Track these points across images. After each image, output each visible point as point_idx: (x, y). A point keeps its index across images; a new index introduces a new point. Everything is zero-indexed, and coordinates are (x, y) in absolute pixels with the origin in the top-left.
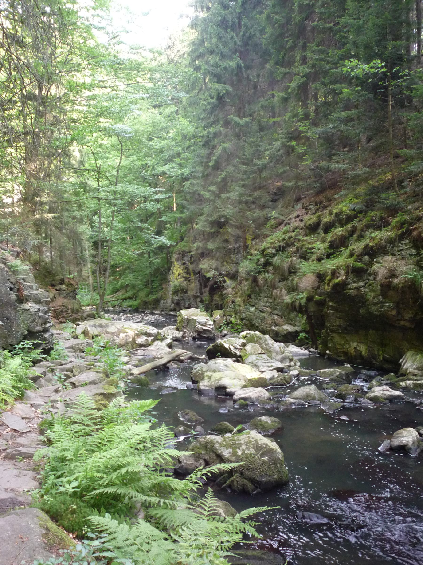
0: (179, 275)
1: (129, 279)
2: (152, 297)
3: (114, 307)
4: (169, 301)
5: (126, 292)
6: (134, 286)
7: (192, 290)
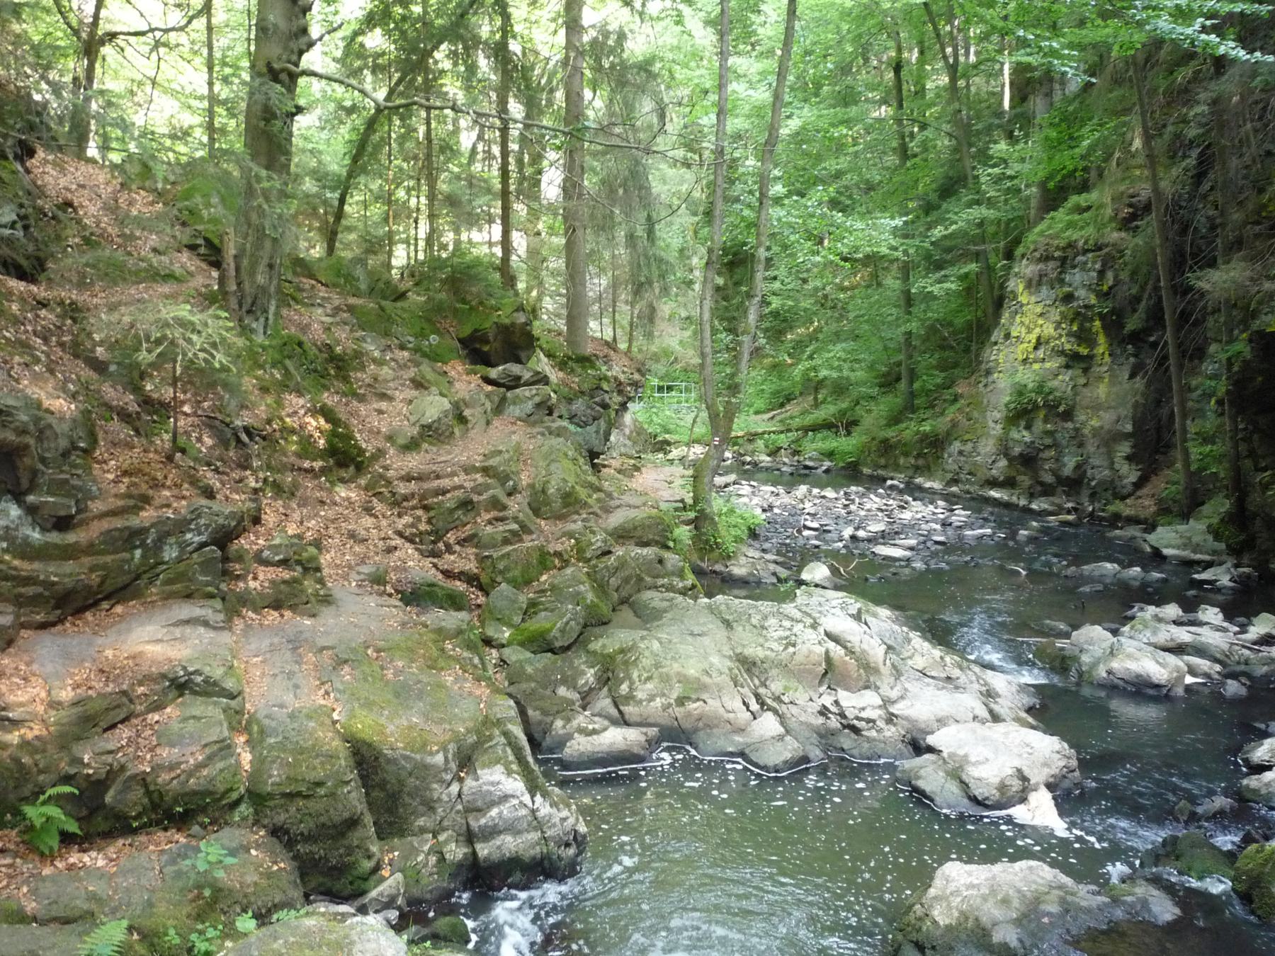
0: (1038, 344)
1: (831, 361)
2: (910, 430)
3: (774, 453)
4: (988, 447)
5: (816, 405)
6: (840, 389)
7: (1096, 407)
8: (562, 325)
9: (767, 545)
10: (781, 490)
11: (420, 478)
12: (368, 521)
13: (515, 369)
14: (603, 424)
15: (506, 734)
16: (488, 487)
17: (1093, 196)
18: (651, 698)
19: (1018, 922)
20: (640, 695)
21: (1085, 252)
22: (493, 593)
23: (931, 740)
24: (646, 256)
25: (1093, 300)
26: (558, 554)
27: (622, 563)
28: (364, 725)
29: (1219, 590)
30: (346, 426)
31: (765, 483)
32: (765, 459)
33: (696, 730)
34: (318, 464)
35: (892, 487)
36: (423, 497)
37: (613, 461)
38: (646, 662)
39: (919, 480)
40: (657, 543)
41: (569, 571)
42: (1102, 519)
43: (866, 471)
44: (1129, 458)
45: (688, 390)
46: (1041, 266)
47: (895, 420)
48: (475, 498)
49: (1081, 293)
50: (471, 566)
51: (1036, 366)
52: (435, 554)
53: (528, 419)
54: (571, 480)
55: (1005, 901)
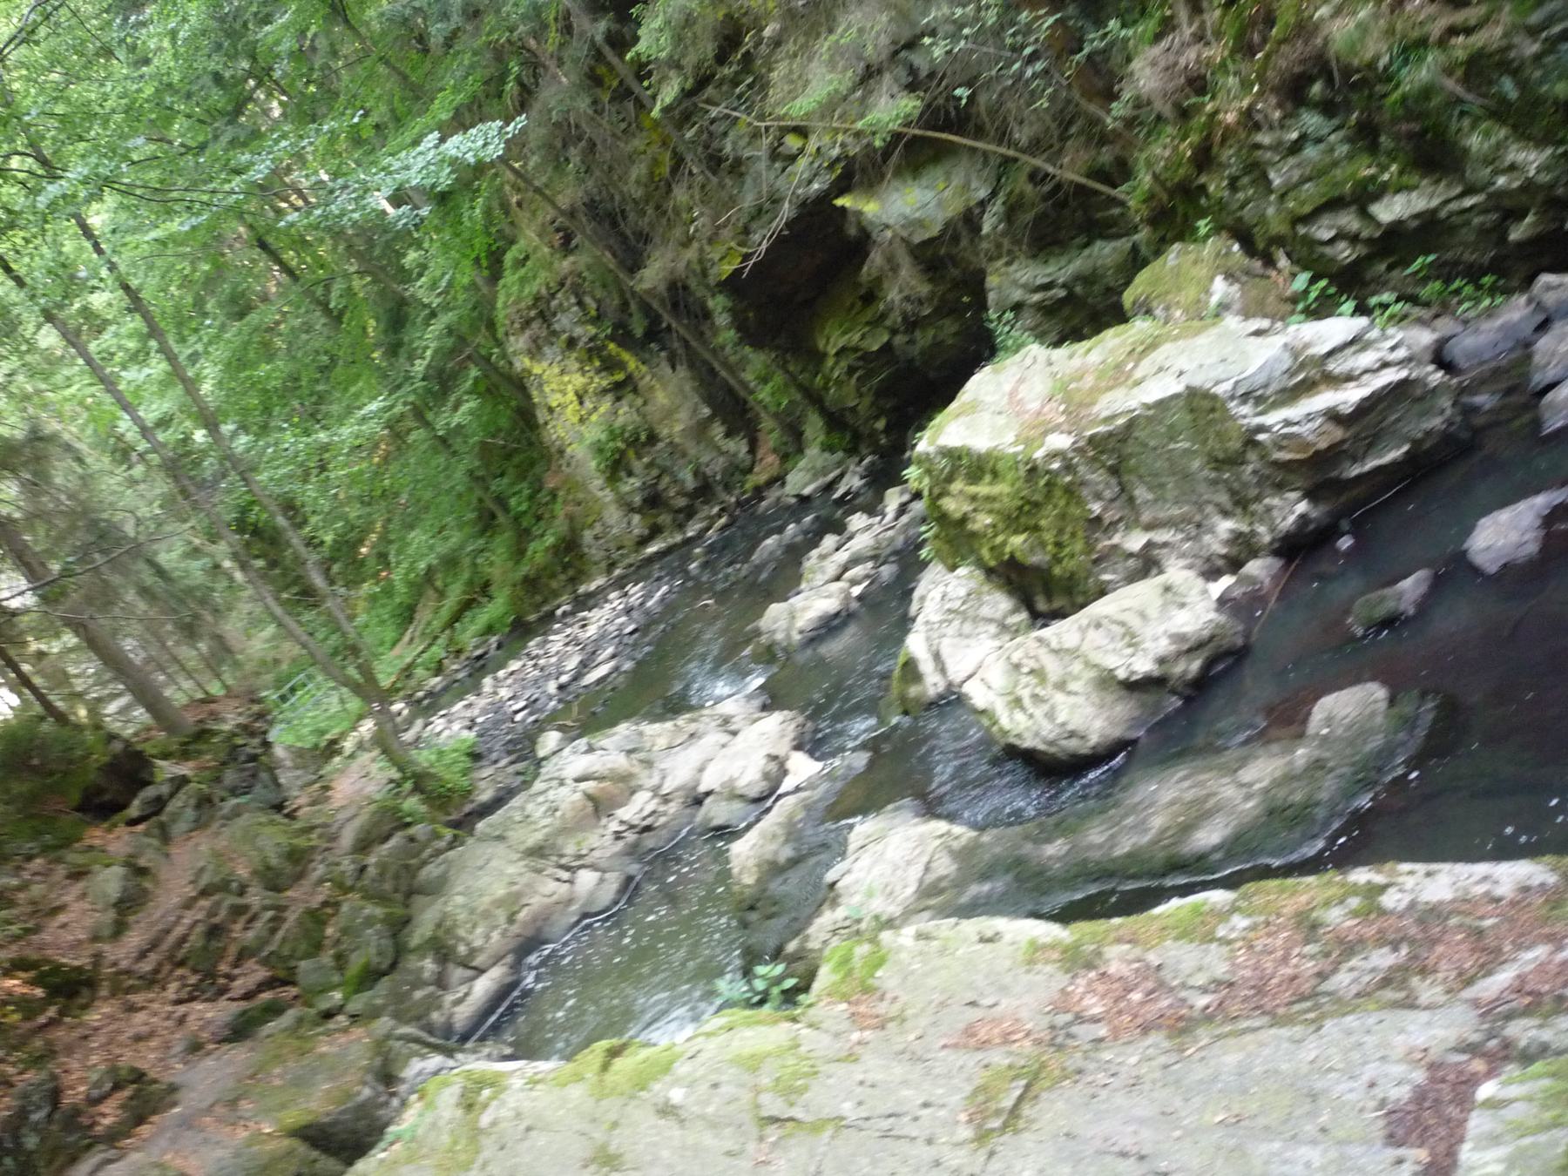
0: (580, 399)
1: (422, 547)
2: (540, 549)
3: (439, 669)
4: (613, 515)
5: (441, 594)
6: (450, 562)
7: (669, 414)
8: (140, 713)
9: (494, 756)
10: (471, 698)
11: (154, 945)
12: (140, 1017)
13: (150, 792)
14: (264, 776)
15: (400, 1038)
16: (218, 904)
17: (522, 243)
18: (487, 937)
19: (787, 841)
20: (478, 943)
21: (553, 296)
22: (300, 978)
23: (702, 788)
24: (173, 596)
25: (592, 330)
26: (325, 904)
27: (383, 867)
28: (294, 1116)
29: (857, 495)
30: (47, 961)
31: (452, 704)
32: (436, 682)
33: (539, 930)
34: (52, 1012)
35: (565, 614)
36: (170, 958)
37: (300, 799)
38: (462, 917)
39: (582, 589)
40: (397, 829)
41: (345, 908)
42: (748, 501)
43: (532, 617)
44: (728, 435)
45: (310, 677)
46: (528, 333)
47: (519, 553)
48: (216, 920)
49: (578, 331)
50: (262, 974)
51: (594, 418)
52: (222, 991)
53: (199, 825)
54: (283, 839)
55: (774, 836)
